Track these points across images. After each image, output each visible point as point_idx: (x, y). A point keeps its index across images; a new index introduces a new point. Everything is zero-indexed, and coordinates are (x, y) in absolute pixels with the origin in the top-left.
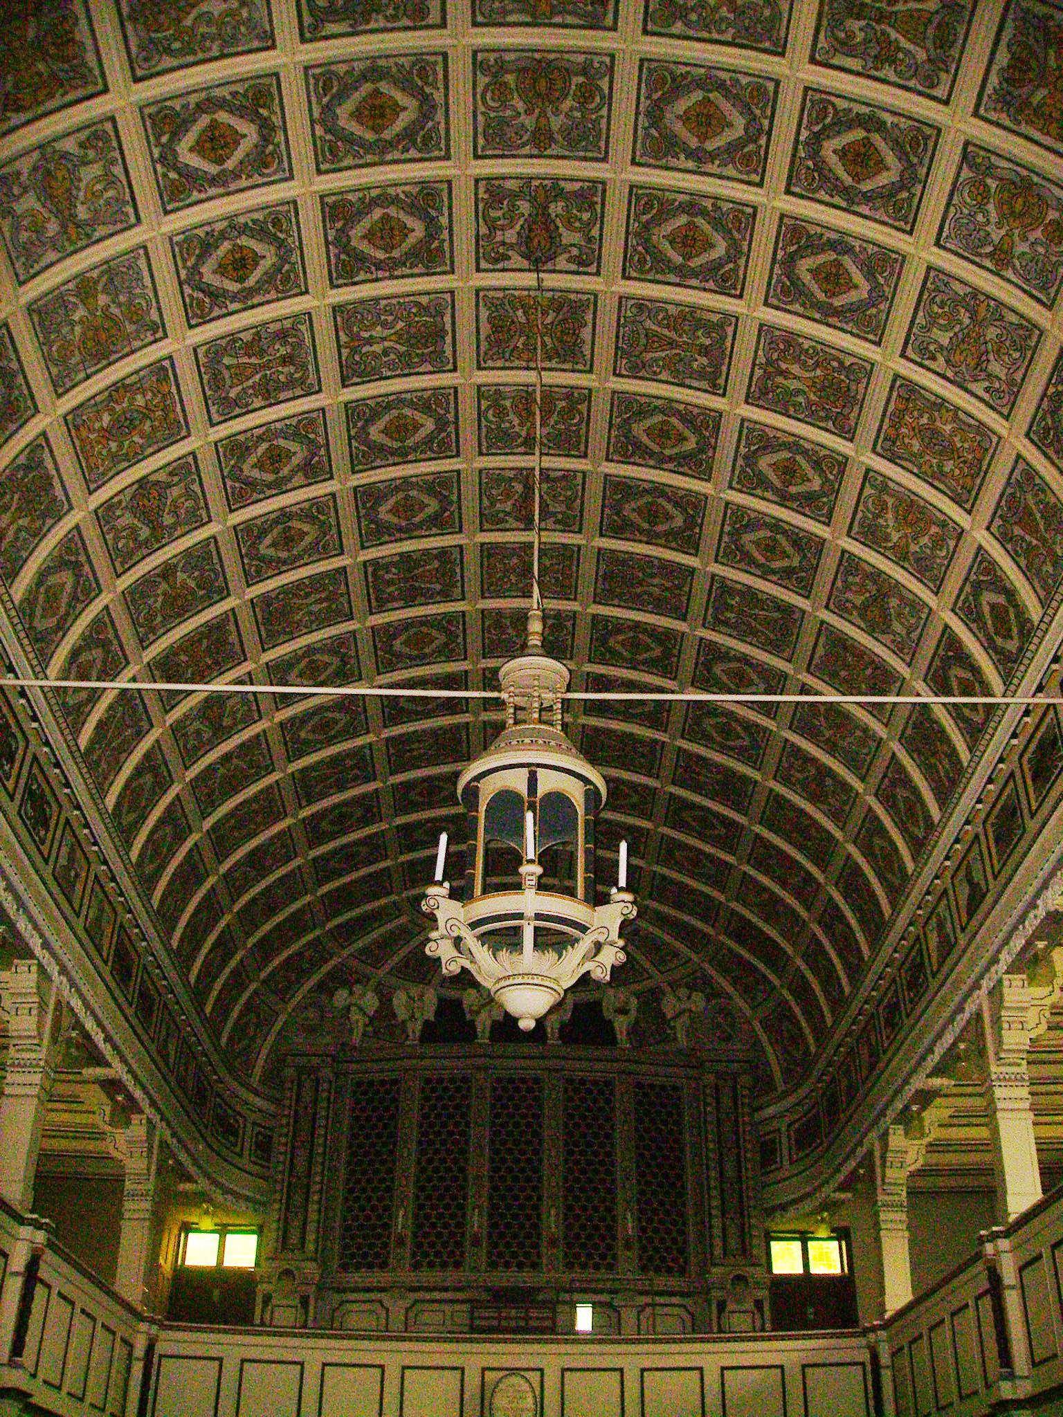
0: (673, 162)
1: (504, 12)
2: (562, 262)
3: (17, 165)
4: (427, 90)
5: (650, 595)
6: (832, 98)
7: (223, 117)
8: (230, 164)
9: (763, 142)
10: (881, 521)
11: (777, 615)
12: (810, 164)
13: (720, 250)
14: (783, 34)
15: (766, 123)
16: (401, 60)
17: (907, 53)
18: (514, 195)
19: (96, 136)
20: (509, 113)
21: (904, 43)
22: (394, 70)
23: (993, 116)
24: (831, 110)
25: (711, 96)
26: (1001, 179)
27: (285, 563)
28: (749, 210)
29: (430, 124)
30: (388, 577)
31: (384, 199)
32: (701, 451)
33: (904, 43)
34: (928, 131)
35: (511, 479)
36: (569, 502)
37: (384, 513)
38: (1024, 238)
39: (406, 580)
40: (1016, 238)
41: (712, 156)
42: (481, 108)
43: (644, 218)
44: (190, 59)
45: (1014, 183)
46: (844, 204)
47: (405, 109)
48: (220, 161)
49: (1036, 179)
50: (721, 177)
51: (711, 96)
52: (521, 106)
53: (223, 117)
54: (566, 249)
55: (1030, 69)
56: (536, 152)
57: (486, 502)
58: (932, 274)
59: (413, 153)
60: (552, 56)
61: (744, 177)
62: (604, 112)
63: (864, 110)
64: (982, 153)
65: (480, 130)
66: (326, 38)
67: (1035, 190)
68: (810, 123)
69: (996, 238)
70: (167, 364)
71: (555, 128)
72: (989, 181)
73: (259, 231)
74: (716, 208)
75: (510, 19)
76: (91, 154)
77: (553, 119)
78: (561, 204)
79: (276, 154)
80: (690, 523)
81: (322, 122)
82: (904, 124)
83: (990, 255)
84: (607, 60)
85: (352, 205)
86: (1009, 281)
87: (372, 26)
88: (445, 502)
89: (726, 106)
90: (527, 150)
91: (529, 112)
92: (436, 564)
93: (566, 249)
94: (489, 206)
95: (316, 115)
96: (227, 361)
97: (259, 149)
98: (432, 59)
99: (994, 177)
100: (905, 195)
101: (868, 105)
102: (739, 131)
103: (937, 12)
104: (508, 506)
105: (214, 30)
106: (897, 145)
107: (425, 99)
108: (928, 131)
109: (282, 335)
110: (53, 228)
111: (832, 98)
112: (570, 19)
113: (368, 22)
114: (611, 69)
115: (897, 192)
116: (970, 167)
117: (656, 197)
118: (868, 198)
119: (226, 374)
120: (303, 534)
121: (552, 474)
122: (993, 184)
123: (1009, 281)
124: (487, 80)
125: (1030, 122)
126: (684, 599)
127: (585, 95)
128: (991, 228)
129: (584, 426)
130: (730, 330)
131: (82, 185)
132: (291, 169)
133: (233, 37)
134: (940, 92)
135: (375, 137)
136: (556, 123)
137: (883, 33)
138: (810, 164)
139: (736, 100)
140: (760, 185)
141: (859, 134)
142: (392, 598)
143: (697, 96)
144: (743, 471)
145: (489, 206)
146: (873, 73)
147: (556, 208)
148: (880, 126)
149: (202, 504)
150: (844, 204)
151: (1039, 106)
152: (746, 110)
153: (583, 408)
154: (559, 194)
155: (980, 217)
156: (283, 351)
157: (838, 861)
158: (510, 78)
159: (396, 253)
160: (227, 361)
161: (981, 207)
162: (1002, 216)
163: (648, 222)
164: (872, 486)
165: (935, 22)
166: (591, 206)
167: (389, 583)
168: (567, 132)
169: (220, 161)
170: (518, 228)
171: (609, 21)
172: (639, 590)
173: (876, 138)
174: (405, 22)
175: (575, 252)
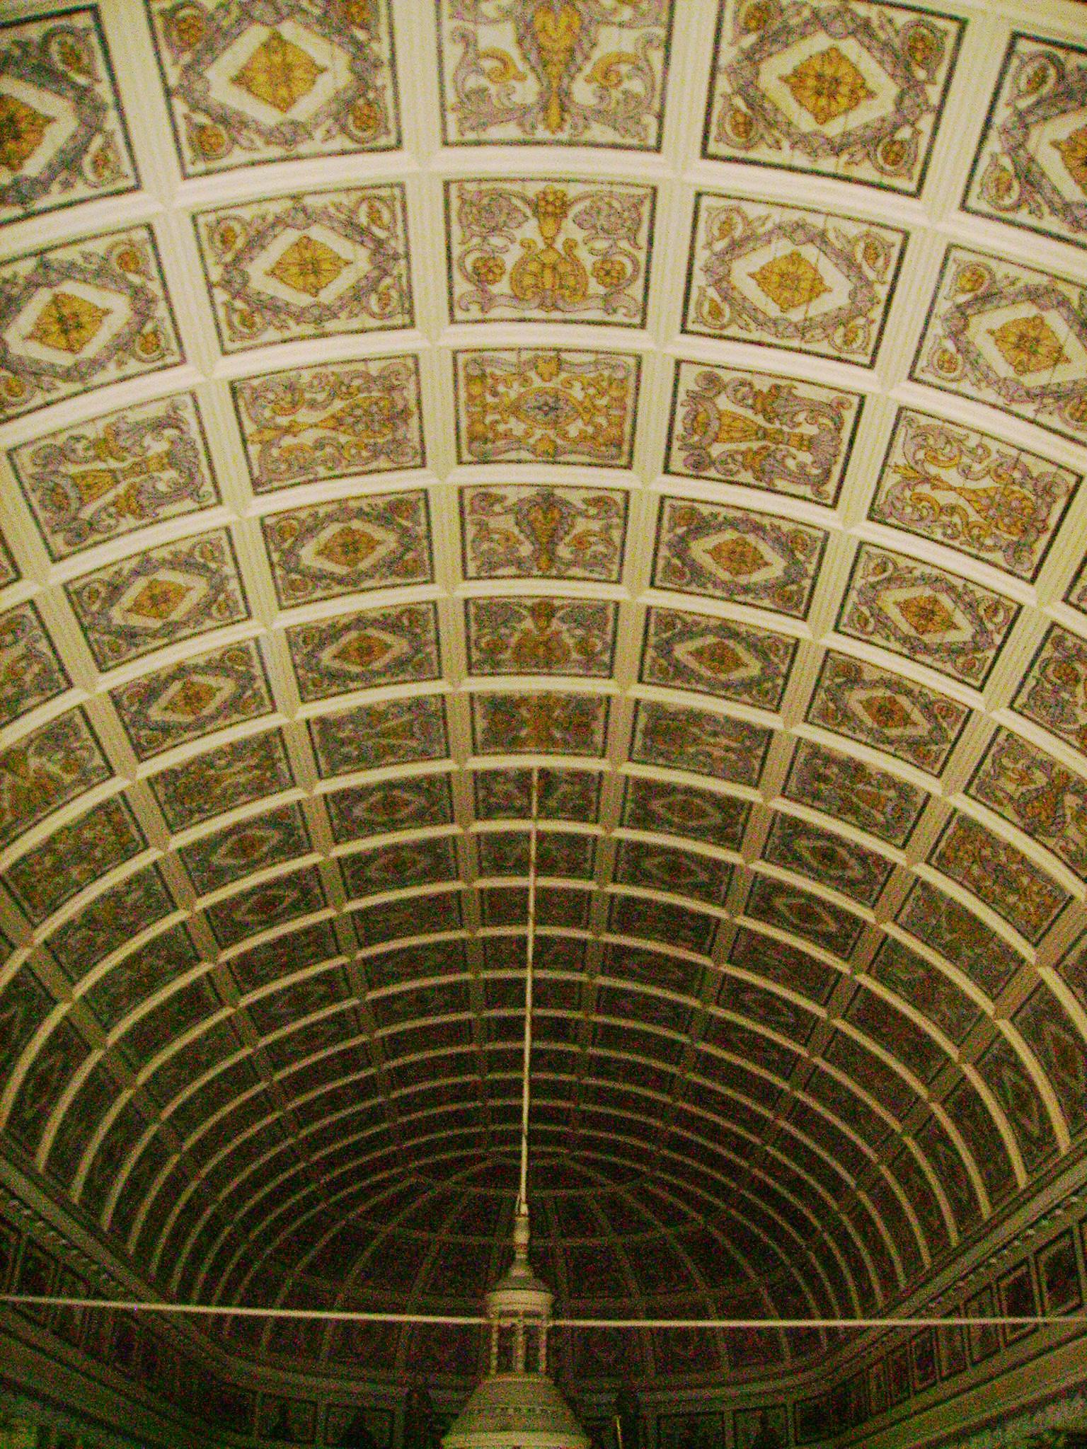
5: (313, 405)
10: (59, 756)
11: (86, 513)
27: (951, 589)
30: (806, 457)
32: (311, 655)
35: (574, 563)
36: (484, 532)
37: (776, 567)
39: (776, 437)
54: (508, 511)
57: (616, 535)
70: (933, 861)
71: (533, 222)
80: (289, 560)
88: (680, 547)
92: (716, 450)
93: (508, 511)
96: (880, 818)
104: (581, 525)
109: (816, 796)
119: (888, 809)
120: (904, 607)
121: (512, 570)
126: (250, 428)
129: (473, 636)
142: (815, 410)
144: (248, 664)
149: (994, 749)
153: (476, 656)
156: (822, 786)
157: (372, 1226)
160: (880, 818)
164: (99, 768)
167: (809, 444)
172: (338, 405)
175: (497, 508)
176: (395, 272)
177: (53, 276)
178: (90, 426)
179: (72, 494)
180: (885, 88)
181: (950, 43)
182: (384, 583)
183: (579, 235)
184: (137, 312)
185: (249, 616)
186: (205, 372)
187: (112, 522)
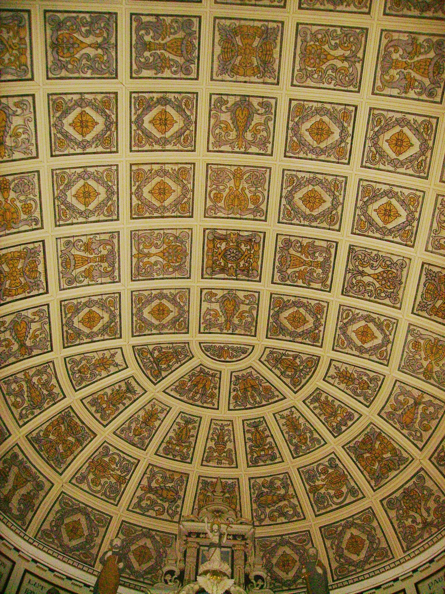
3: (5, 319)
19: (41, 311)
24: (351, 313)
31: (161, 296)
73: (102, 305)
76: (37, 318)
103: (433, 58)
106: (417, 131)
110: (15, 347)
130: (333, 251)
131: (12, 127)
135: (160, 204)
165: (433, 63)
176: (188, 197)
177: (86, 176)
178: (85, 237)
179: (73, 263)
180: (311, 320)
181: (325, 309)
182: (173, 214)
183: (246, 186)
184: (106, 126)
185: (121, 337)
186: (127, 341)
187: (83, 279)
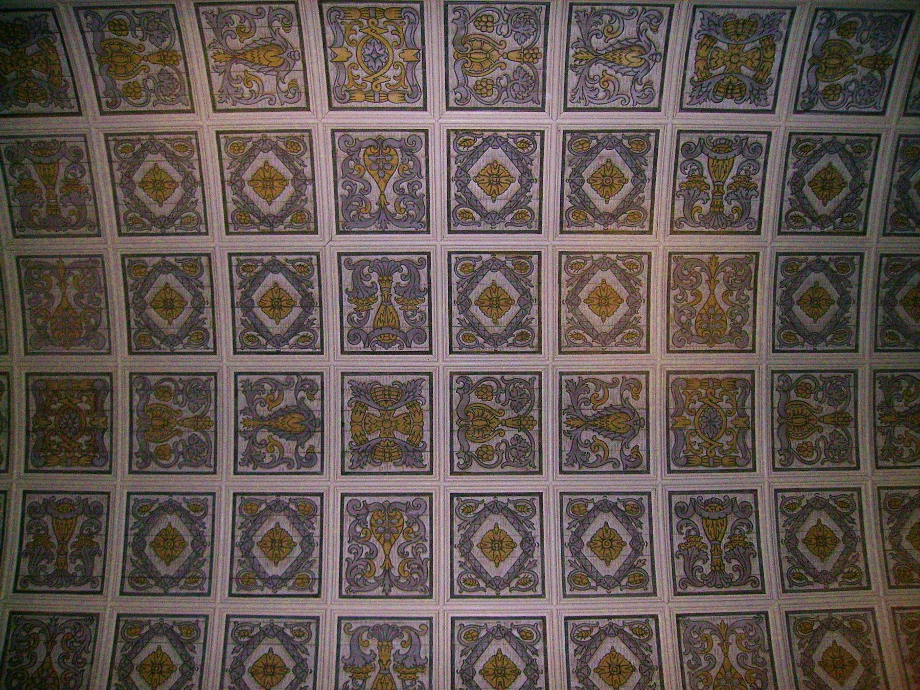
0: (853, 322)
1: (746, 449)
2: (637, 404)
4: (804, 503)
6: (784, 213)
7: (818, 655)
8: (857, 657)
9: (826, 258)
12: (838, 220)
13: (498, 277)
14: (743, 256)
15: (811, 258)
16: (781, 523)
17: (740, 168)
18: (576, 442)
20: (821, 444)
21: (733, 173)
22: (788, 527)
23: (771, 99)
25: (795, 300)
26: (817, 80)
28: (564, 257)
29: (831, 502)
33: (733, 173)
34: (794, 141)
38: (860, 50)
40: (861, 56)
41: (843, 293)
42: (818, 465)
43: (902, 338)
44: (770, 674)
45: (463, 66)
46: (866, 190)
47: (819, 521)
48: (853, 663)
49: (809, 56)
50: (860, 285)
51: (795, 300)
52: (816, 435)
53: (818, 655)
55: (730, 82)
56: (853, 424)
58: (909, 111)
59: (855, 516)
60: (776, 415)
61: (857, 267)
62: (817, 375)
63: (788, 190)
64: (801, 99)
65: (835, 466)
66: (762, 575)
67: (818, 53)
68: (806, 226)
69: (865, 71)
71: (832, 410)
72: (821, 88)
74: (886, 284)
75: (749, 445)
77: (825, 412)
78: (896, 403)
79: (851, 620)
81: (827, 582)
82: (792, 159)
83: (882, 71)
84: (776, 376)
85: (897, 565)
86: (899, 51)
87: (755, 542)
89: (802, 290)
90: (851, 431)
91: (820, 430)
94: (585, 463)
95: (821, 586)
97: (846, 632)
98: (780, 500)
99: (817, 86)
100: (848, 147)
101: (783, 188)
102: (821, 276)
103: (707, 155)
105: (750, 655)
106: (811, 161)
107: (810, 506)
108: (794, 141)
111: (784, 213)
112: (748, 403)
113: (752, 544)
114: (783, 372)
115: (847, 152)
116: (813, 106)
117: (883, 330)
118: (857, 174)
122: (822, 86)
123: (899, 51)
124: (796, 460)
125: (768, 72)
127: (804, 389)
128: (858, 77)
132: (865, 609)
133: (757, 641)
134: (763, 140)
136: (827, 409)
137: (729, 188)
138: (838, 220)
139: (796, 282)
140: (862, 255)
141: (807, 189)
143: (797, 309)
145: (585, 463)
146: (759, 189)
147: (899, 406)
148: (798, 176)
150: (866, 190)
151: (755, 69)
152: (803, 273)
154: (888, 404)
155: (504, 82)
158: (794, 444)
159: (840, 535)
161: (843, 89)
162: (847, 71)
163: (904, 335)
166: (896, 380)
168: (833, 402)
169: (853, 663)
170: (606, 440)
171: (748, 377)
173: (808, 177)
174: (752, 519)
